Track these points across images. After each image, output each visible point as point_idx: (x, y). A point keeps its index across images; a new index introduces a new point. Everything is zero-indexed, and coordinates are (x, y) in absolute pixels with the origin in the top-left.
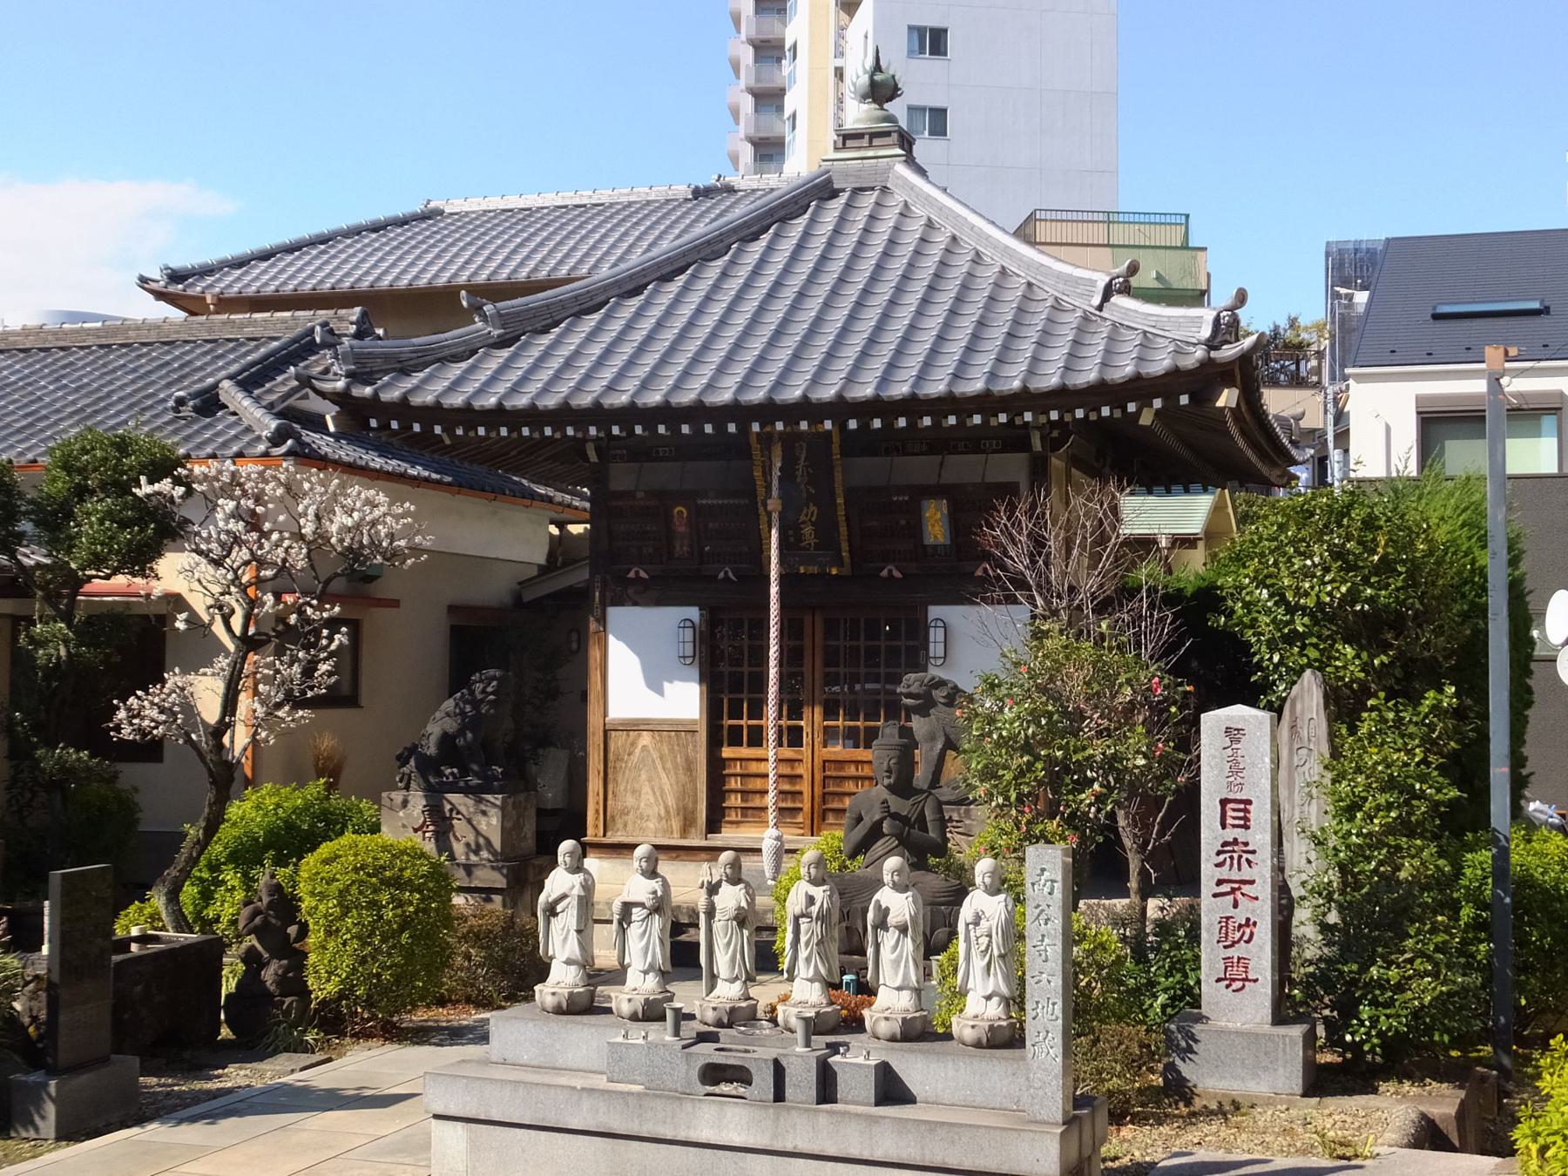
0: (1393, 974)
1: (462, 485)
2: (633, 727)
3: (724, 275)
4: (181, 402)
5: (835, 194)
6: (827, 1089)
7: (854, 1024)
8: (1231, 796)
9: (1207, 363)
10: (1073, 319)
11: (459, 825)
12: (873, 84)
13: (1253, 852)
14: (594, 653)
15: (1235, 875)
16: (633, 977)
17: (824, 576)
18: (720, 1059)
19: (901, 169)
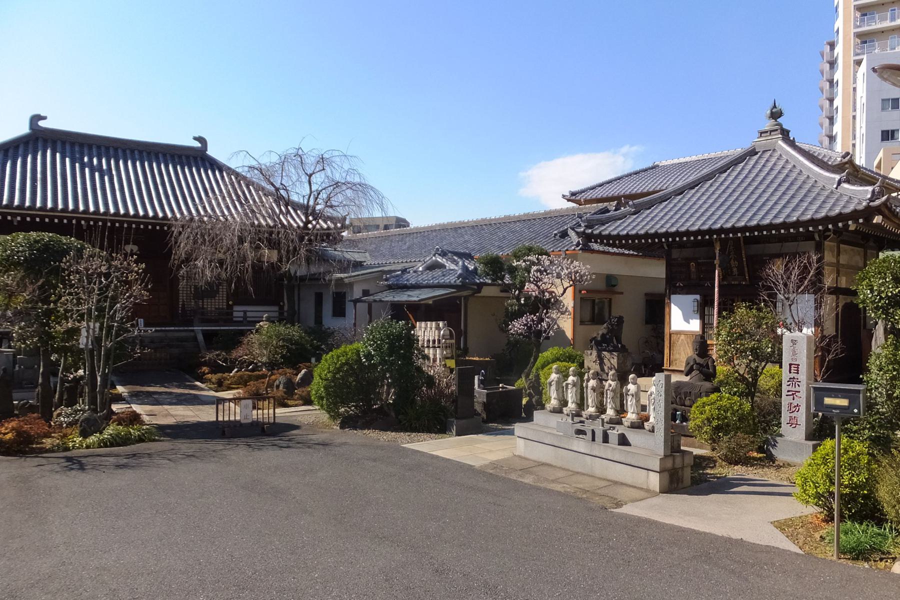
0: (855, 428)
1: (645, 256)
2: (679, 333)
3: (711, 185)
4: (556, 235)
5: (756, 153)
6: (606, 439)
7: (620, 423)
9: (868, 207)
10: (826, 193)
11: (606, 361)
12: (772, 113)
14: (667, 310)
16: (570, 404)
17: (740, 285)
18: (582, 428)
19: (780, 143)
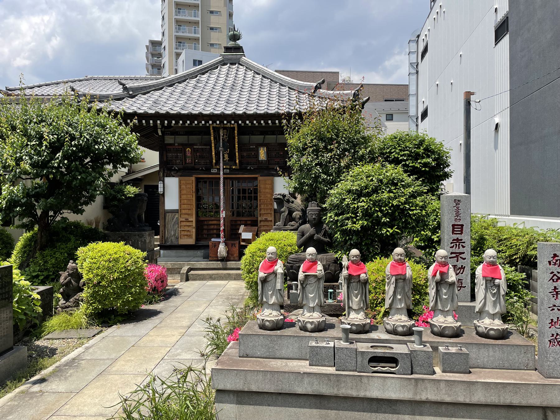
8: (456, 223)
13: (464, 242)
15: (457, 250)
